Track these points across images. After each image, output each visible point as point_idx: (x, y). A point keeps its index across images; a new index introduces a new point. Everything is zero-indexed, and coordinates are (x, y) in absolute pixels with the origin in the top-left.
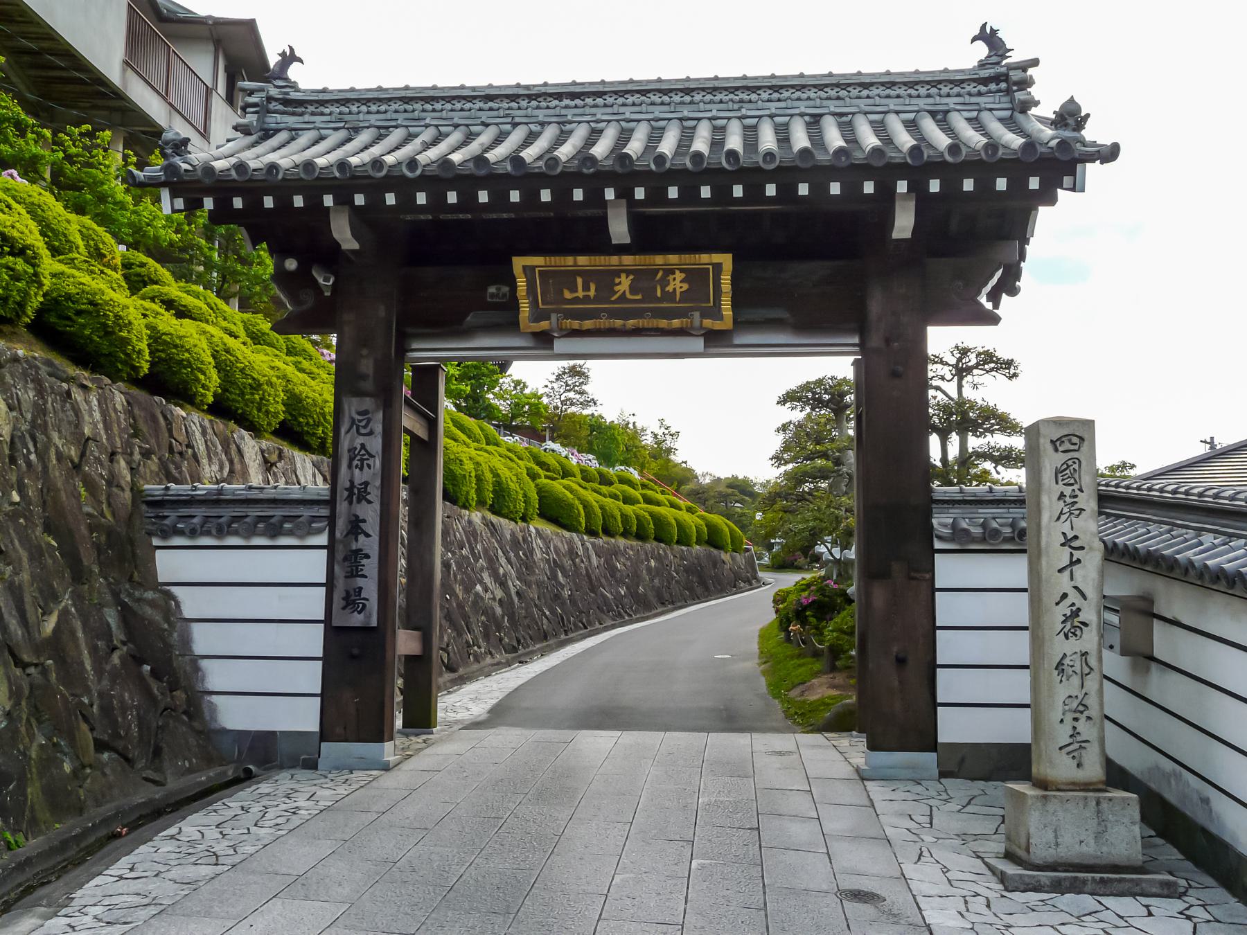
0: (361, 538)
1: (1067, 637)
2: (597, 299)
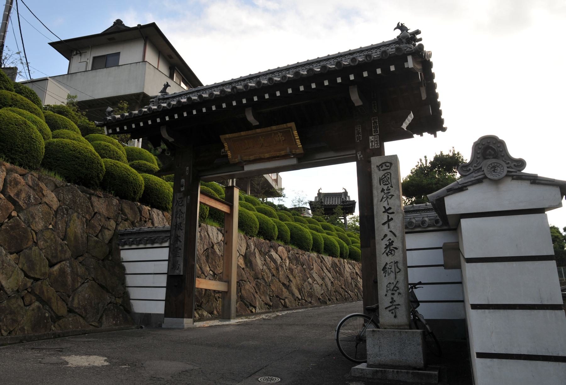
0: (179, 242)
1: (387, 254)
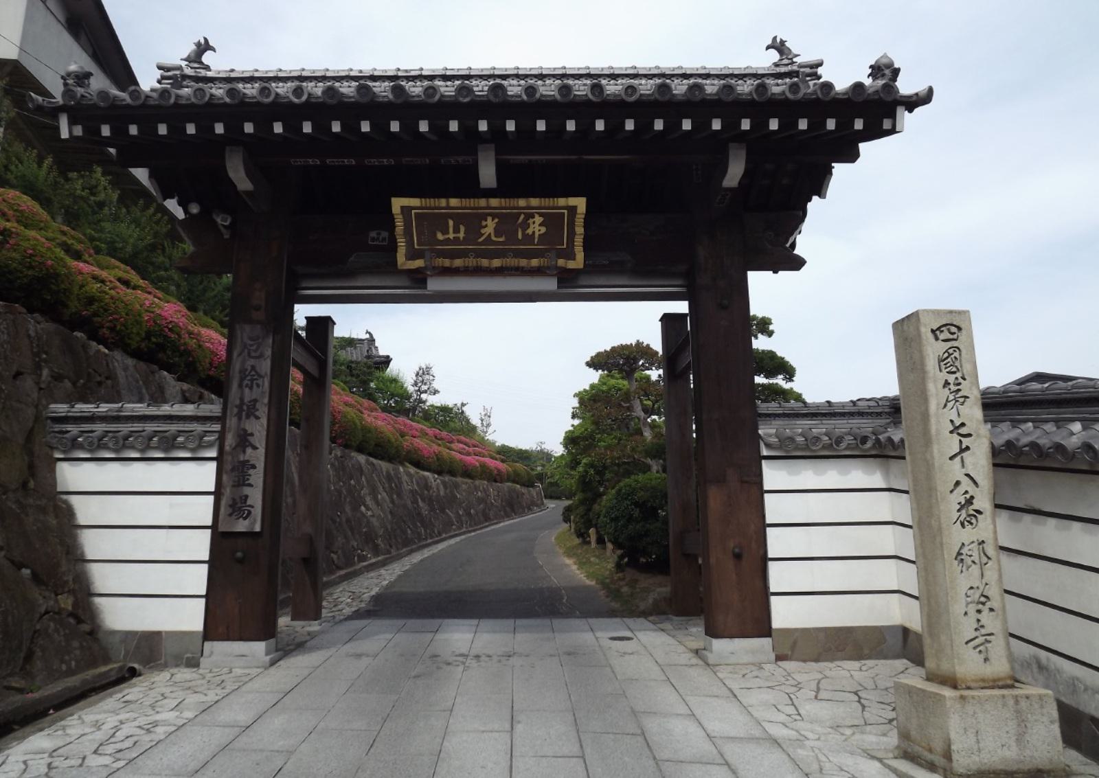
0: (249, 450)
1: (963, 525)
2: (466, 241)
